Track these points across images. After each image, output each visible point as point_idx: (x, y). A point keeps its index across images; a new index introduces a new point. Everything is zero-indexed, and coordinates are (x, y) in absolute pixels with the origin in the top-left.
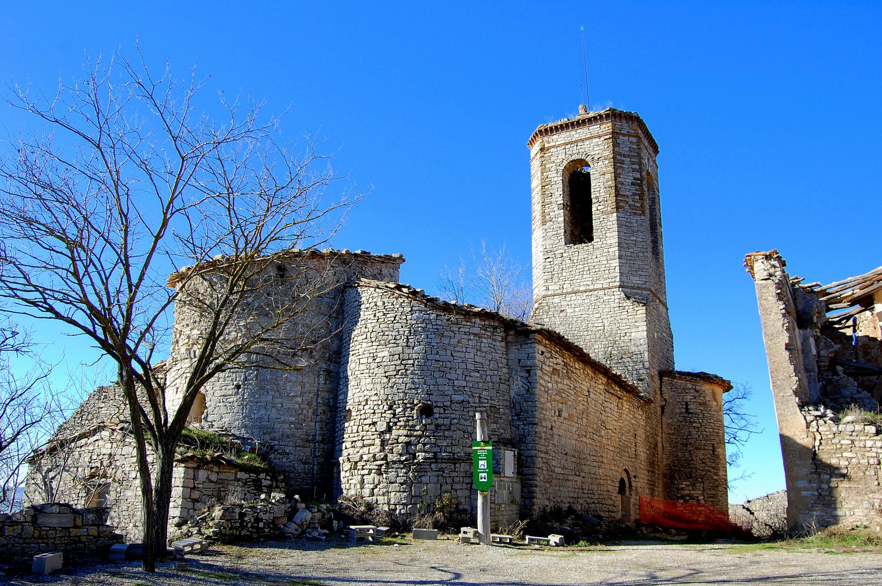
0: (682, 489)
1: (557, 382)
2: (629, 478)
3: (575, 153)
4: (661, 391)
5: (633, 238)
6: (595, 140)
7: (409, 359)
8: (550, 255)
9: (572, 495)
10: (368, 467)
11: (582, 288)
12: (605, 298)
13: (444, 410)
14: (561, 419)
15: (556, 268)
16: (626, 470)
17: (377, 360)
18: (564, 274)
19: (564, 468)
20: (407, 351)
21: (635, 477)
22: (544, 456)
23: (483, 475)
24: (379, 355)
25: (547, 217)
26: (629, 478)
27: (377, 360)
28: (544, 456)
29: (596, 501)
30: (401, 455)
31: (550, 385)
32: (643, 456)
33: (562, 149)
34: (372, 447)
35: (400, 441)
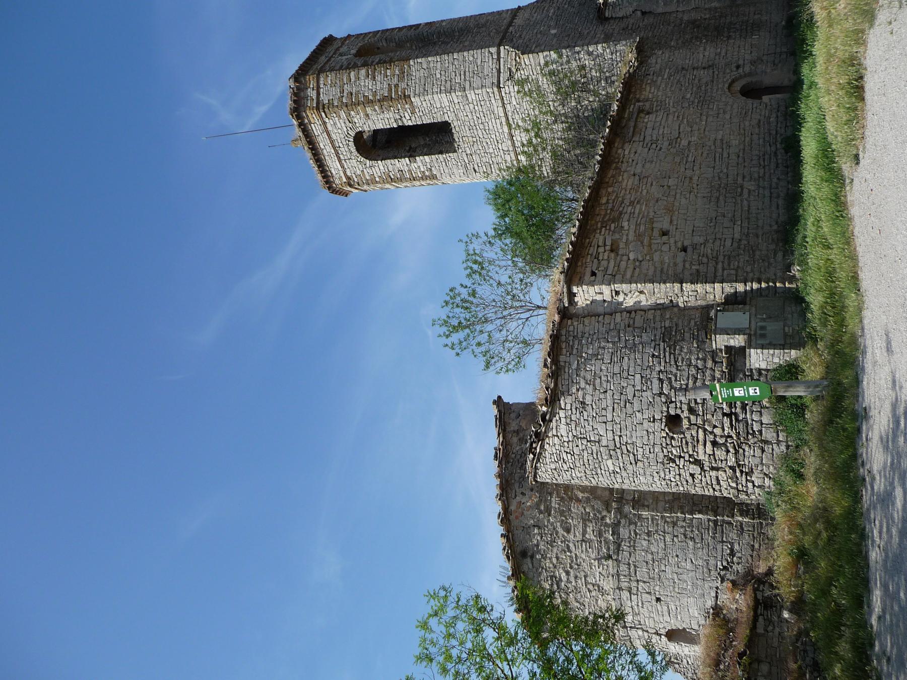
1: (627, 243)
2: (741, 77)
3: (349, 149)
4: (622, 18)
5: (438, 76)
6: (330, 128)
8: (470, 167)
9: (767, 200)
11: (506, 129)
12: (515, 103)
13: (672, 402)
14: (672, 229)
15: (484, 160)
16: (729, 88)
18: (491, 150)
20: (604, 443)
21: (738, 67)
22: (720, 266)
23: (751, 392)
24: (611, 468)
25: (427, 173)
26: (741, 77)
28: (720, 266)
29: (773, 149)
30: (728, 451)
31: (632, 256)
33: (347, 164)
34: (720, 478)
35: (711, 453)
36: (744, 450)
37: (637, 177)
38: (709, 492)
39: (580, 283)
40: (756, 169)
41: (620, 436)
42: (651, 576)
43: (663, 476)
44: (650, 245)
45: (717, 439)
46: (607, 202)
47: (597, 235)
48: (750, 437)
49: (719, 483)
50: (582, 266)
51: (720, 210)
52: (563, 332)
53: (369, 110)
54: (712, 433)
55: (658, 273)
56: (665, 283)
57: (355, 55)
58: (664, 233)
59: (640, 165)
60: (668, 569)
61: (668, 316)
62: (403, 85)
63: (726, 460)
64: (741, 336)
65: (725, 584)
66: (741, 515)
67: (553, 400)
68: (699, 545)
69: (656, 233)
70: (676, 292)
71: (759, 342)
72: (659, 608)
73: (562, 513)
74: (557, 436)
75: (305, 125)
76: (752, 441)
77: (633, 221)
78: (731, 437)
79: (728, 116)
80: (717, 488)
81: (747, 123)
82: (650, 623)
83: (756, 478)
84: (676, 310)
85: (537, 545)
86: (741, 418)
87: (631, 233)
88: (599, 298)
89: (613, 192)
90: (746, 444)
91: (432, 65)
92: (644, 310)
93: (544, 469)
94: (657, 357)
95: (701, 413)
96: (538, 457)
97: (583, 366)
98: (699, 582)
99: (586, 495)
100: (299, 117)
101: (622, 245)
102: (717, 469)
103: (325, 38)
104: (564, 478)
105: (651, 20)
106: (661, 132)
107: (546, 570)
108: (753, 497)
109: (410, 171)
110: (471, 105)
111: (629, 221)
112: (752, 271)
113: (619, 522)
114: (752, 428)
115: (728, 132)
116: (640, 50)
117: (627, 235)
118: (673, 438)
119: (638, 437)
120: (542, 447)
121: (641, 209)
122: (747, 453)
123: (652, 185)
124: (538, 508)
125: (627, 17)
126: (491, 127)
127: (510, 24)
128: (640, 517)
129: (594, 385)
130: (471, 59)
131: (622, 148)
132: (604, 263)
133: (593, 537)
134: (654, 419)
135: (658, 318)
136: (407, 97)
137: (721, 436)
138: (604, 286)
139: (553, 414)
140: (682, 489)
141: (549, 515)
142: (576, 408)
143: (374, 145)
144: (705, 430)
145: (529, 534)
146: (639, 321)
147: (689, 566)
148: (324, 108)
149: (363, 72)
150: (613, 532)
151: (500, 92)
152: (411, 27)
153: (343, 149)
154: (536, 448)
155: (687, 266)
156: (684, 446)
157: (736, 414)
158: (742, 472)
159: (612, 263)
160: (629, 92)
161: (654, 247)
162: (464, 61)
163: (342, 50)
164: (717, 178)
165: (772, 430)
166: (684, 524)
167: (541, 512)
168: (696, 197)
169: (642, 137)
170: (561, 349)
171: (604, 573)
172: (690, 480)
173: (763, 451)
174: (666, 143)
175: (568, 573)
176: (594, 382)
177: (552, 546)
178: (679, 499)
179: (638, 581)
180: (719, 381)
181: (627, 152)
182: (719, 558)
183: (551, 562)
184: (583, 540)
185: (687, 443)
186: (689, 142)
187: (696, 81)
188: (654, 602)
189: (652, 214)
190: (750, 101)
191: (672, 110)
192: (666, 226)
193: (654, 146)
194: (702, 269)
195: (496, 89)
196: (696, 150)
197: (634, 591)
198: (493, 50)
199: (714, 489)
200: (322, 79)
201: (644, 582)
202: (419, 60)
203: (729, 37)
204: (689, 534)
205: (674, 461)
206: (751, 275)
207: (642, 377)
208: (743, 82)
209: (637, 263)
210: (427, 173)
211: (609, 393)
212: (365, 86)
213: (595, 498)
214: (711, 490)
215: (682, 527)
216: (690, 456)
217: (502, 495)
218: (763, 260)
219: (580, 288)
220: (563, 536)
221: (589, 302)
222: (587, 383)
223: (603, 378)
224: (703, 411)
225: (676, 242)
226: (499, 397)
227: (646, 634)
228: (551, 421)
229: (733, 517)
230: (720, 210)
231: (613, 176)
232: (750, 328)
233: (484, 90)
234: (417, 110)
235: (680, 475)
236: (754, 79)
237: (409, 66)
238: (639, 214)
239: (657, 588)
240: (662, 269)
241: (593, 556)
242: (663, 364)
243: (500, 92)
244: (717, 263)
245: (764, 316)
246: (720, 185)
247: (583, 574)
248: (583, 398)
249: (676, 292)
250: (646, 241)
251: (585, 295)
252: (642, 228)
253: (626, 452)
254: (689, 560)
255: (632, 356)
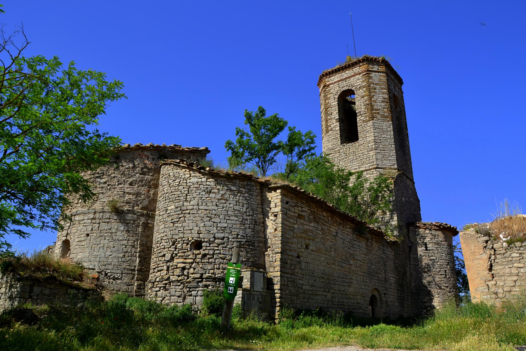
0: (425, 302)
1: (303, 224)
2: (380, 295)
4: (409, 236)
5: (383, 136)
6: (357, 77)
7: (187, 210)
10: (159, 285)
13: (210, 244)
16: (376, 289)
17: (168, 212)
18: (341, 163)
19: (312, 286)
20: (185, 204)
21: (385, 294)
22: (290, 276)
23: (231, 279)
24: (169, 208)
25: (329, 128)
26: (380, 295)
27: (168, 212)
28: (290, 276)
30: (179, 276)
31: (296, 226)
32: (392, 280)
33: (336, 85)
35: (178, 266)
36: (179, 286)
37: (335, 234)
38: (152, 266)
39: (282, 194)
40: (337, 300)
41: (189, 213)
42: (102, 232)
43: (164, 238)
44: (301, 237)
45: (186, 270)
46: (324, 216)
47: (307, 208)
48: (188, 289)
49: (159, 271)
50: (291, 196)
51: (318, 279)
52: (253, 183)
53: (366, 98)
54: (191, 267)
55: (287, 240)
56: (281, 243)
57: (394, 94)
58: (307, 247)
59: (342, 236)
60: (106, 241)
61: (260, 245)
62: (379, 117)
63: (173, 275)
64: (249, 286)
65: (97, 274)
66: (138, 285)
67: (213, 175)
68: (120, 260)
69: (307, 241)
70: (275, 250)
71: (246, 295)
72: (83, 236)
73: (141, 181)
74: (190, 176)
75: (359, 63)
76: (185, 290)
77: (314, 229)
78: (188, 278)
79: (363, 287)
80: (156, 270)
81: (359, 297)
82: (74, 230)
83: (162, 293)
84: (264, 250)
85: (122, 166)
86: (199, 284)
87: (307, 227)
88: (272, 205)
89: (329, 220)
90: (183, 287)
91: (389, 133)
92: (264, 232)
93: (169, 169)
94: (237, 237)
95: (203, 261)
96: (177, 165)
97: (233, 193)
98: (98, 259)
99: (152, 196)
100: (364, 60)
101: (302, 221)
102: (168, 270)
103: (402, 80)
104: (162, 181)
105: (407, 251)
106: (357, 250)
107: (107, 170)
108: (149, 291)
109: (331, 119)
110: (367, 153)
111: (314, 227)
112: (286, 294)
113: (135, 214)
114: (193, 291)
115: (356, 286)
116: (395, 243)
117: (307, 225)
118: (187, 244)
119: (189, 224)
120: (184, 167)
121: (320, 234)
122: (177, 287)
123: (332, 242)
124: (144, 168)
125: (409, 238)
126: (354, 163)
127: (407, 177)
128: (138, 226)
129: (221, 199)
130: (392, 154)
131: (350, 228)
132: (293, 210)
133: (126, 198)
134: (199, 234)
135: (259, 239)
136: (372, 118)
137: (188, 273)
138: (280, 208)
139: (204, 174)
140: (155, 250)
141: (141, 174)
142: (207, 188)
143: (345, 101)
144: (192, 263)
145: (130, 161)
146: (258, 228)
147: (108, 253)
148: (368, 74)
149: (386, 96)
150: (130, 210)
151: (374, 169)
152: (406, 125)
153: (345, 83)
154: (183, 163)
155: (290, 257)
156: (182, 251)
157: (201, 281)
158: (166, 284)
159: (293, 214)
160: (376, 235)
161: (300, 240)
162: (390, 150)
163: (396, 87)
164: (333, 278)
165: (192, 302)
166: (133, 252)
167: (142, 169)
168: (325, 266)
169: (355, 239)
170: (243, 181)
171: (105, 204)
172: (161, 254)
173: (179, 297)
174: (352, 252)
175: (105, 183)
176: (223, 199)
177: (121, 174)
178: (148, 250)
179: (99, 223)
180: (222, 272)
181: (348, 230)
182: (112, 271)
183: (112, 173)
184: (124, 192)
185: (184, 252)
186: (351, 265)
187: (380, 272)
188: (86, 233)
189: (317, 240)
190: (369, 299)
191: (367, 257)
192: (311, 247)
193: (351, 245)
194: (288, 266)
195: (375, 166)
196: (348, 268)
197: (94, 221)
198: (396, 166)
199: (155, 269)
200: (383, 74)
201: (99, 227)
202: (391, 127)
203: (398, 290)
204: (127, 254)
205: (173, 245)
206: (284, 293)
207: (225, 227)
208: (378, 296)
209: (292, 229)
210: (329, 128)
211: (216, 208)
212: (379, 97)
213: (150, 201)
214: (154, 267)
215: (131, 251)
216: (176, 254)
217: (153, 146)
218: (291, 301)
219: (279, 194)
220: (128, 181)
221: (270, 199)
222: (222, 195)
223: (225, 205)
224: (204, 262)
225: (302, 252)
226: (209, 152)
227: (67, 228)
228: (200, 173)
229: (137, 280)
230: (318, 279)
231: (336, 221)
232: (254, 291)
233: (375, 160)
234: (365, 124)
235: (164, 248)
236: (379, 302)
237: (388, 121)
238: (318, 233)
239: (95, 235)
240: (288, 243)
241: (115, 198)
242: (233, 240)
243: (374, 169)
244: (291, 274)
245: (260, 300)
246: (330, 280)
247: (104, 192)
248: (213, 192)
249: (275, 250)
250: (303, 235)
251: (275, 198)
252: (310, 234)
253: (179, 216)
254: (111, 253)
255: (238, 222)
